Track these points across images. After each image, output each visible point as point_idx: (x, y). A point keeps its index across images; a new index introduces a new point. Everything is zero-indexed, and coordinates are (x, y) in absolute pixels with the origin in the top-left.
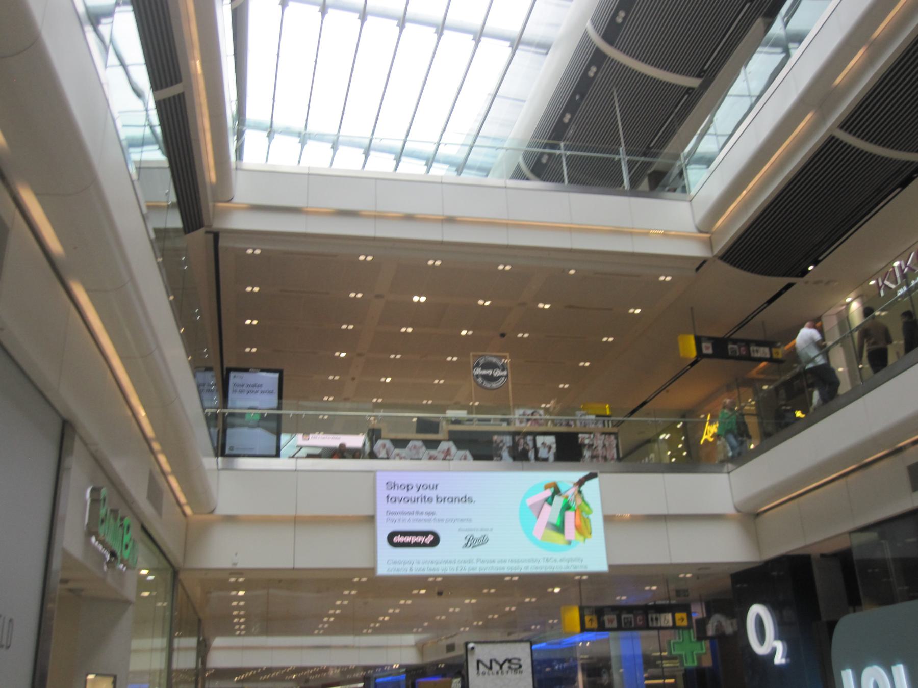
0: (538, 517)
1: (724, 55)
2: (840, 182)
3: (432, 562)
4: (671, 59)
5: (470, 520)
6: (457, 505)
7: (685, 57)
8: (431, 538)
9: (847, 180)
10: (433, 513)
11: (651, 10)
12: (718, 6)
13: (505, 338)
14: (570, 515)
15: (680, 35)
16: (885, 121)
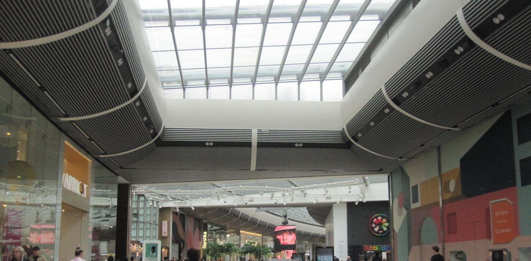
2: (425, 115)
11: (426, 105)
12: (473, 74)
16: (423, 108)
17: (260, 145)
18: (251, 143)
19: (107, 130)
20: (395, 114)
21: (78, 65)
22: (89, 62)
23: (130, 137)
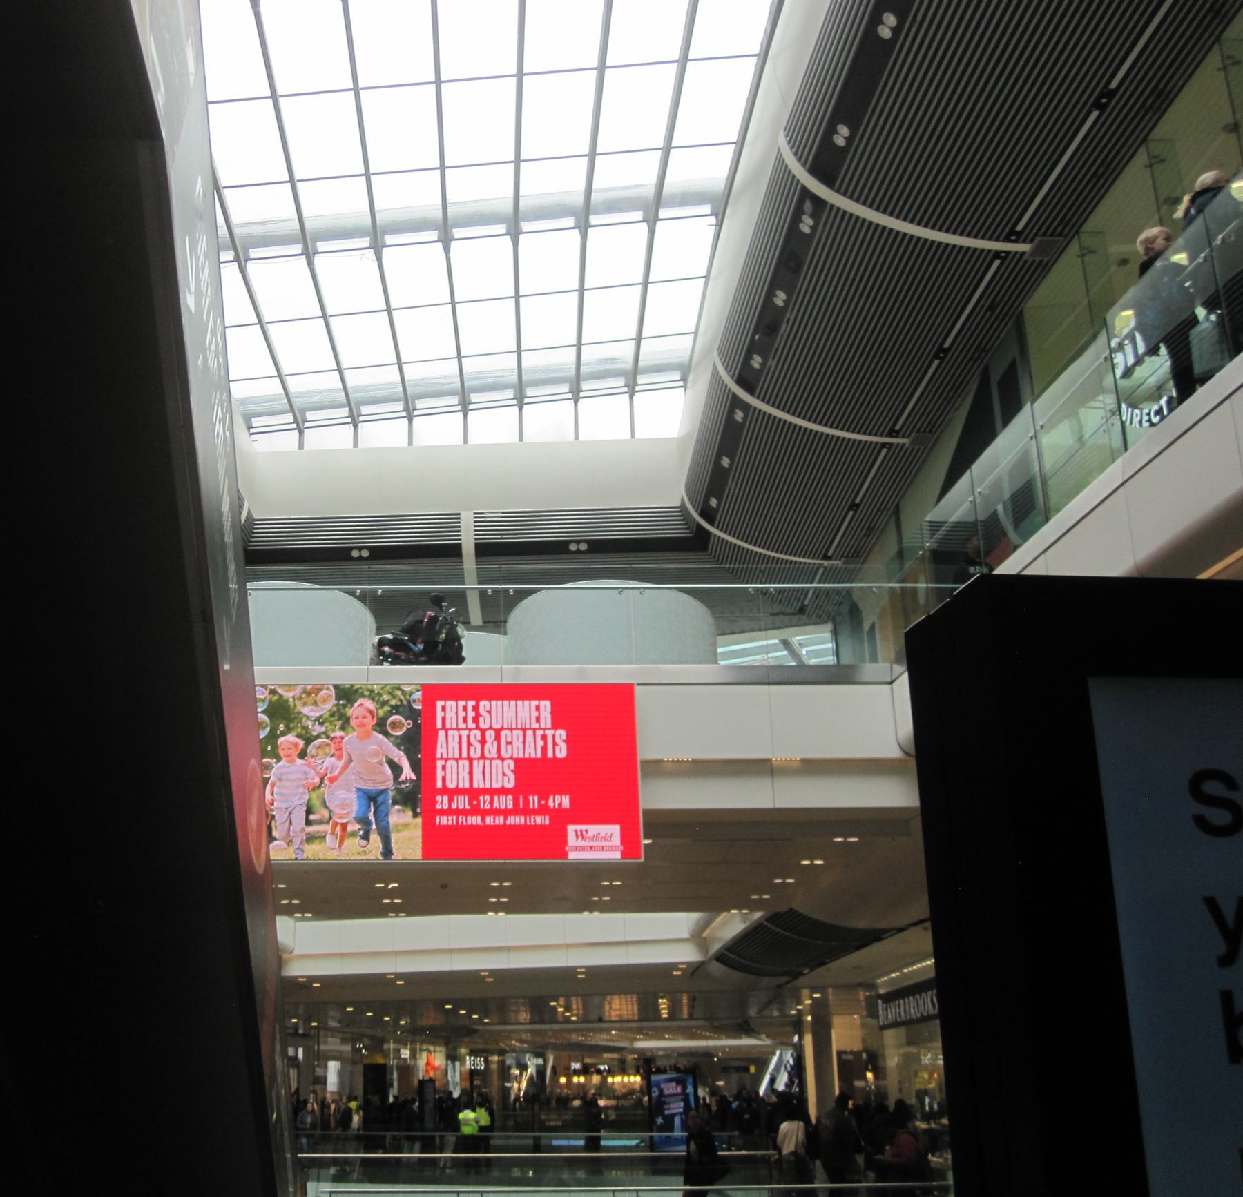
1: (937, 381)
4: (797, 530)
9: (827, 493)
11: (811, 509)
13: (785, 638)
17: (482, 550)
18: (459, 547)
20: (884, 425)
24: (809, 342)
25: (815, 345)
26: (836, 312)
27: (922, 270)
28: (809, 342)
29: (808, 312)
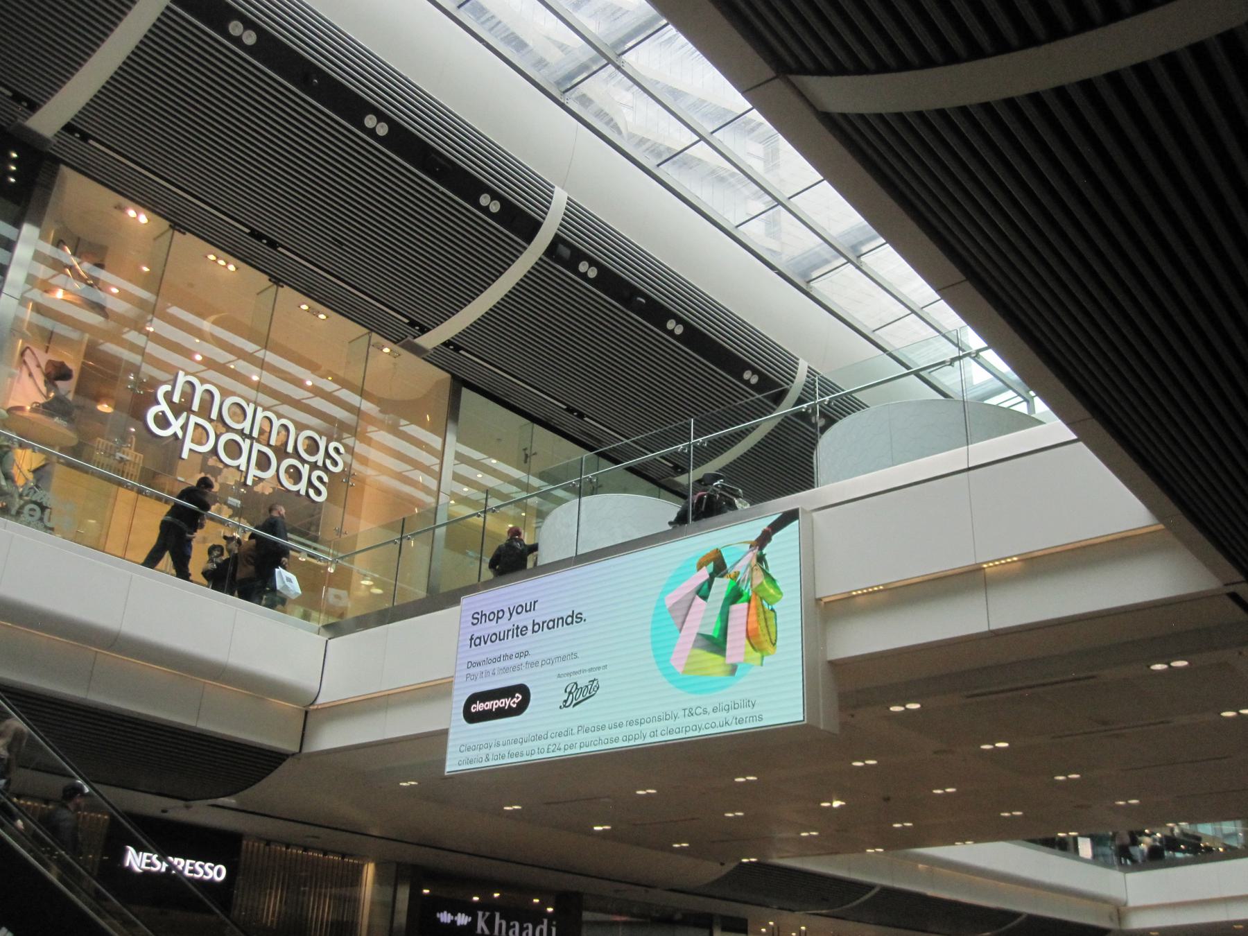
0: (680, 630)
3: (515, 742)
5: (574, 656)
6: (562, 630)
7: (616, 364)
8: (519, 697)
9: (219, 230)
10: (526, 654)
14: (739, 609)
15: (133, 128)
19: (668, 387)
21: (615, 377)
22: (139, 119)
23: (777, 443)
24: (409, 280)
25: (226, 159)
26: (396, 236)
27: (613, 351)
28: (409, 280)
29: (737, 389)
